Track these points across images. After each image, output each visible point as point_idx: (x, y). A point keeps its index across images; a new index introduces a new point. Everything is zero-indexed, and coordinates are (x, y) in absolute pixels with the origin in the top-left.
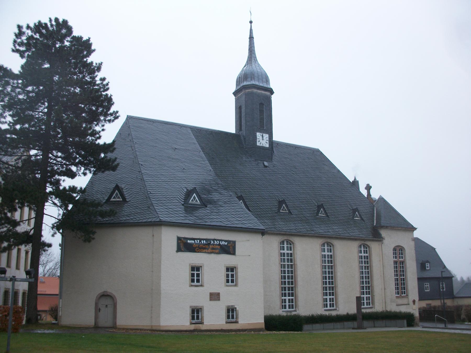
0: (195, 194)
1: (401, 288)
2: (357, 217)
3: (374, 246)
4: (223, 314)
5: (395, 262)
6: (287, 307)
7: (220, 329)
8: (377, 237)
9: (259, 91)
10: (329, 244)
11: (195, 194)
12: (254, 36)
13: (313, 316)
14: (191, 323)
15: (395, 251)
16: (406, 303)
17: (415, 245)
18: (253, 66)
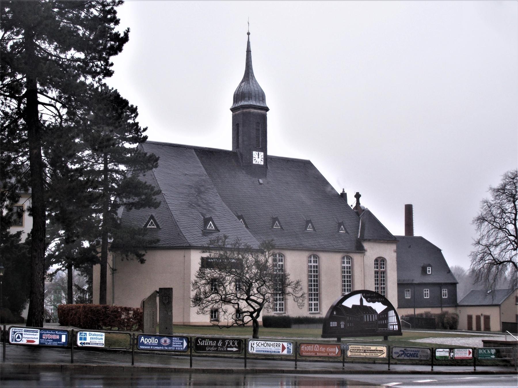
2: (342, 230)
3: (357, 258)
5: (376, 272)
6: (313, 309)
9: (255, 110)
10: (315, 256)
13: (299, 318)
14: (211, 321)
15: (377, 261)
18: (251, 83)
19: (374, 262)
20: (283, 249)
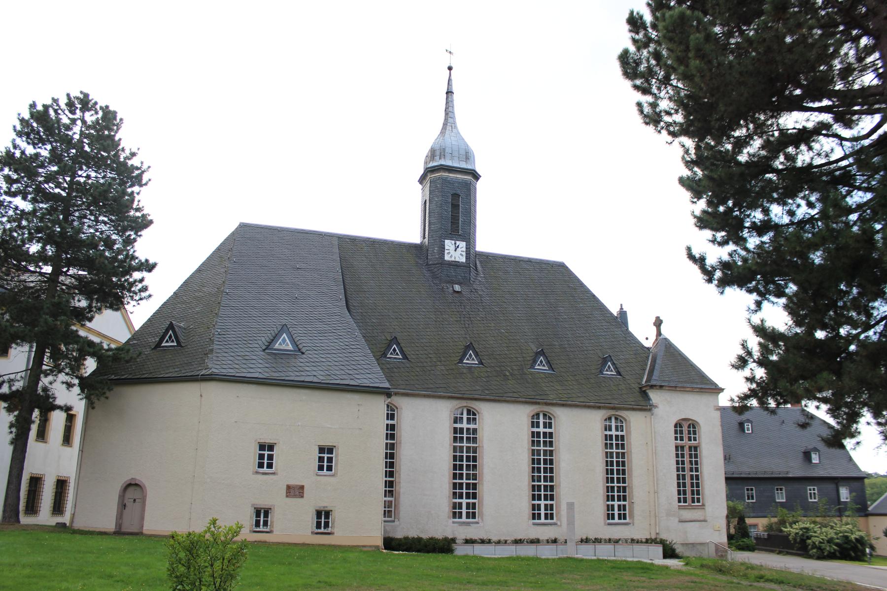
0: (284, 335)
1: (689, 490)
3: (636, 421)
4: (311, 519)
7: (301, 542)
8: (644, 405)
11: (284, 335)
12: (454, 90)
16: (702, 518)
17: (722, 417)
19: (673, 429)
20: (476, 399)
